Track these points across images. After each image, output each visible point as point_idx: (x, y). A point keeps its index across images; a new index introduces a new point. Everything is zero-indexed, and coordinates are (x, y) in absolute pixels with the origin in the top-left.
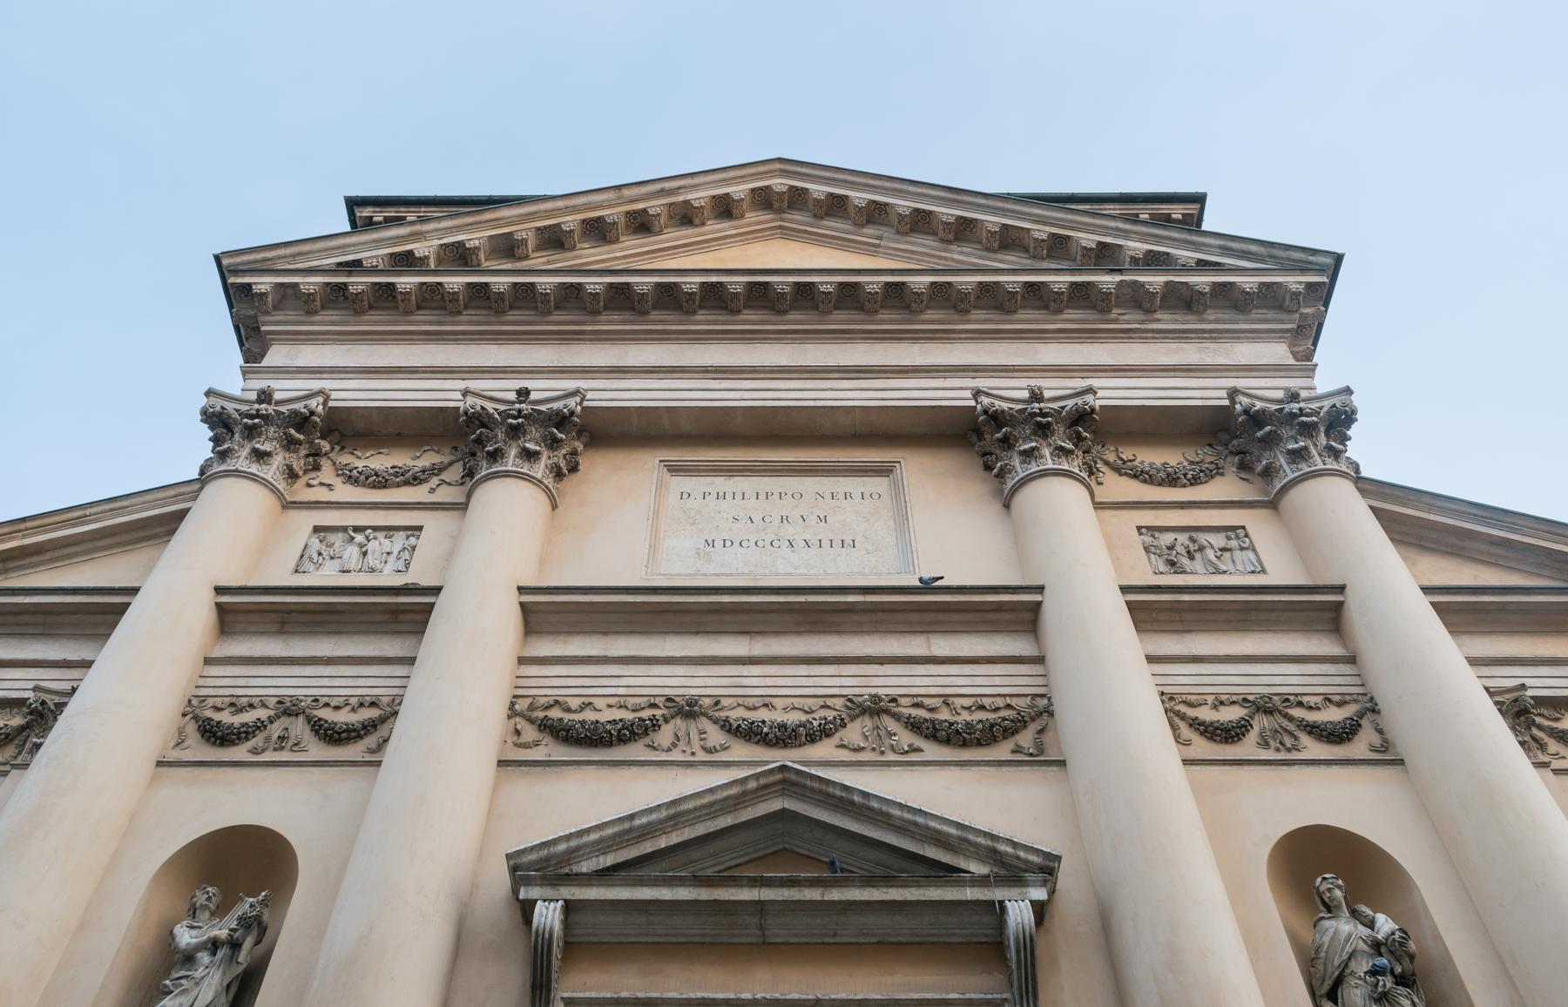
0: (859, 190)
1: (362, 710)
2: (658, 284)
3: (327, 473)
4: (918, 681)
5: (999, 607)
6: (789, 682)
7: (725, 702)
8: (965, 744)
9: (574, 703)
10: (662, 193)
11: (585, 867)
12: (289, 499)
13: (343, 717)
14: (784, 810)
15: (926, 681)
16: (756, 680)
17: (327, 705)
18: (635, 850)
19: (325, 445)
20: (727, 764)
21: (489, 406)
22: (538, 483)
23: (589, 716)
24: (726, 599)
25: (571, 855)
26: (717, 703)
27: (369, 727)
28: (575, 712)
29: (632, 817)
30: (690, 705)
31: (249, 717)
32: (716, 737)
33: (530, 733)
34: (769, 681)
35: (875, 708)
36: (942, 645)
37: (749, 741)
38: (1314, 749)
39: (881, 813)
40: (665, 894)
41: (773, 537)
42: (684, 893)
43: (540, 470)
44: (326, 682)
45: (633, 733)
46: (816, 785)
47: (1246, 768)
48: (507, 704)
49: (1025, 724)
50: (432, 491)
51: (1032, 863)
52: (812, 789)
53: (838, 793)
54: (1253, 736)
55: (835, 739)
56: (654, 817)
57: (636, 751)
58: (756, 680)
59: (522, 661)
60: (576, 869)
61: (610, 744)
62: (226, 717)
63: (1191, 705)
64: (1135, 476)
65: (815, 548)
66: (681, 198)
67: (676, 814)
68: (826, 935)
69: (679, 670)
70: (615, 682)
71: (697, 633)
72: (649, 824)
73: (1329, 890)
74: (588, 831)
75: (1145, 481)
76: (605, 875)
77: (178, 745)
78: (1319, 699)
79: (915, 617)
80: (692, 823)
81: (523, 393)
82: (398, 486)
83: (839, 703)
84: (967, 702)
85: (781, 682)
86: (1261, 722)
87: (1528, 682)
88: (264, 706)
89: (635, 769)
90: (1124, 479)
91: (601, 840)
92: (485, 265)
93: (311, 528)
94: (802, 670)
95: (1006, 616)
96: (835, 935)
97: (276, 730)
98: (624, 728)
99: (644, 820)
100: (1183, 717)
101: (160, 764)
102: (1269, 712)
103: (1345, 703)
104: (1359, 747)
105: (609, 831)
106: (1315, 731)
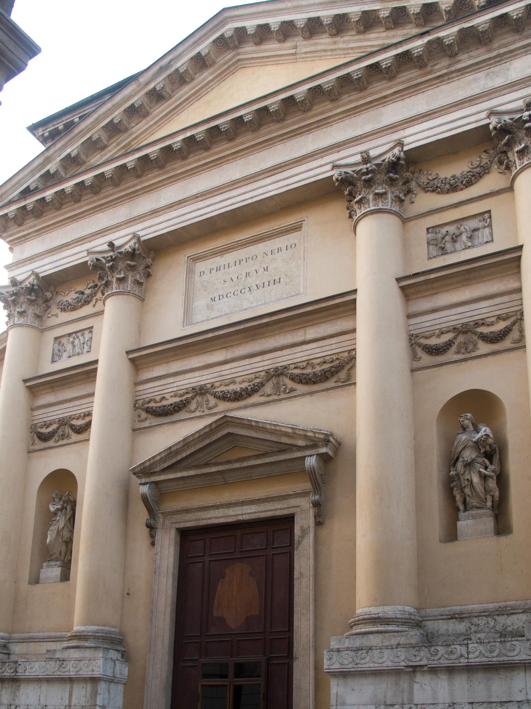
0: (274, 16)
2: (162, 149)
3: (54, 310)
4: (298, 355)
5: (337, 306)
6: (241, 369)
7: (216, 384)
8: (314, 383)
9: (158, 398)
10: (162, 70)
11: (158, 469)
13: (433, 341)
14: (229, 433)
15: (301, 354)
16: (227, 371)
17: (74, 419)
18: (176, 459)
19: (48, 295)
20: (215, 414)
21: (349, 170)
23: (165, 403)
24: (210, 335)
25: (152, 466)
26: (212, 386)
28: (158, 402)
29: (170, 448)
30: (200, 390)
31: (50, 429)
32: (213, 401)
33: (144, 415)
34: (233, 371)
35: (278, 373)
36: (312, 333)
37: (225, 401)
38: (484, 348)
39: (263, 428)
40: (185, 474)
41: (242, 287)
42: (192, 473)
43: (129, 285)
44: (71, 409)
45: (179, 407)
46: (238, 421)
48: (132, 405)
49: (343, 367)
50: (94, 306)
51: (321, 438)
52: (237, 423)
53: (246, 423)
55: (260, 393)
56: (178, 446)
57: (182, 415)
58: (227, 371)
60: (155, 470)
61: (172, 414)
62: (44, 430)
63: (426, 338)
64: (433, 191)
65: (261, 288)
66: (173, 69)
67: (186, 442)
68: (248, 477)
69: (197, 374)
70: (171, 386)
71: (204, 353)
72: (177, 449)
74: (156, 456)
75: (439, 193)
76: (164, 470)
77: (32, 444)
78: (494, 319)
79: (298, 320)
80: (195, 445)
81: (111, 245)
82: (81, 307)
83: (263, 374)
84: (318, 361)
85: (237, 370)
86: (461, 339)
87: (224, 373)
88: (55, 423)
89: (181, 423)
91: (161, 459)
92: (108, 144)
93: (53, 339)
94: (247, 361)
95: (341, 309)
96: (251, 477)
97: (60, 432)
98: (175, 406)
99: (175, 448)
101: (29, 452)
105: (163, 455)
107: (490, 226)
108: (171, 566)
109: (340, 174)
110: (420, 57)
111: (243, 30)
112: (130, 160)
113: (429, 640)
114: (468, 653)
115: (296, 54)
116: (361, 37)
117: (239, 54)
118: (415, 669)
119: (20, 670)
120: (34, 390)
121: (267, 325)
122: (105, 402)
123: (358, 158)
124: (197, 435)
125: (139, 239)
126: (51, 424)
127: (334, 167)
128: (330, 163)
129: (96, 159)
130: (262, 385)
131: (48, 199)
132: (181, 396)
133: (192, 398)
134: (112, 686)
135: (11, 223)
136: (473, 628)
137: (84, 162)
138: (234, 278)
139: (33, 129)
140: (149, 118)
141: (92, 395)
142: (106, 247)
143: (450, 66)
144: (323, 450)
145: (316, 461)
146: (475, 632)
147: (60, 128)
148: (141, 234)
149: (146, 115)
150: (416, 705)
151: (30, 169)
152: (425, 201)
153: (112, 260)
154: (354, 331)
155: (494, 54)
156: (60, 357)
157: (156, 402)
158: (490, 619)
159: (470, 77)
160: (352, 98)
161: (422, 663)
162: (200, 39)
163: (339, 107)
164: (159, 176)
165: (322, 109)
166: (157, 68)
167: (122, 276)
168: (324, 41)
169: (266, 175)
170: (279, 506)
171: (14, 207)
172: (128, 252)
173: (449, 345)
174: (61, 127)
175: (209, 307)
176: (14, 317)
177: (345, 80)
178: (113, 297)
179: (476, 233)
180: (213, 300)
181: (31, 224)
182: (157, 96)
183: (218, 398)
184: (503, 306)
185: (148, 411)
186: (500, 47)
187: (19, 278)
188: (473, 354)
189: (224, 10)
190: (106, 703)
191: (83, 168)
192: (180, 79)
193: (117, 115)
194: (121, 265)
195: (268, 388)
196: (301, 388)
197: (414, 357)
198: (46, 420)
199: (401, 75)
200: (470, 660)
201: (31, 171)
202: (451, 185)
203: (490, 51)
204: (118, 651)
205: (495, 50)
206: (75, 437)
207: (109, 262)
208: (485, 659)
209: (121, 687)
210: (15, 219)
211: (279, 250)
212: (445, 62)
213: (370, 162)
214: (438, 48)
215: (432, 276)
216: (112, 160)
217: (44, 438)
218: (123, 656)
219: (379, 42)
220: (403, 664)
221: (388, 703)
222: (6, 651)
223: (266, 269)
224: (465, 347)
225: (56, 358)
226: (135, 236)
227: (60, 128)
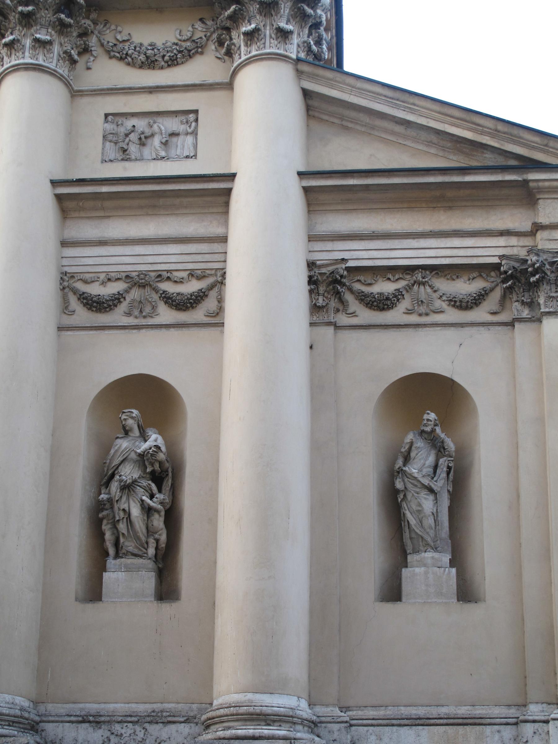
1: (110, 284)
12: (75, 88)
13: (95, 290)
17: (168, 278)
22: (52, 73)
27: (197, 299)
38: (166, 315)
47: (107, 332)
54: (123, 307)
59: (64, 244)
63: (86, 282)
64: (121, 59)
73: (125, 419)
75: (128, 64)
78: (184, 274)
86: (135, 294)
90: (114, 62)
100: (75, 291)
102: (143, 286)
103: (204, 277)
104: (198, 315)
106: (171, 301)
107: (195, 133)
152: (106, 72)
184: (199, 258)
197: (66, 309)
202: (148, 58)
215: (105, 189)
224: (139, 308)
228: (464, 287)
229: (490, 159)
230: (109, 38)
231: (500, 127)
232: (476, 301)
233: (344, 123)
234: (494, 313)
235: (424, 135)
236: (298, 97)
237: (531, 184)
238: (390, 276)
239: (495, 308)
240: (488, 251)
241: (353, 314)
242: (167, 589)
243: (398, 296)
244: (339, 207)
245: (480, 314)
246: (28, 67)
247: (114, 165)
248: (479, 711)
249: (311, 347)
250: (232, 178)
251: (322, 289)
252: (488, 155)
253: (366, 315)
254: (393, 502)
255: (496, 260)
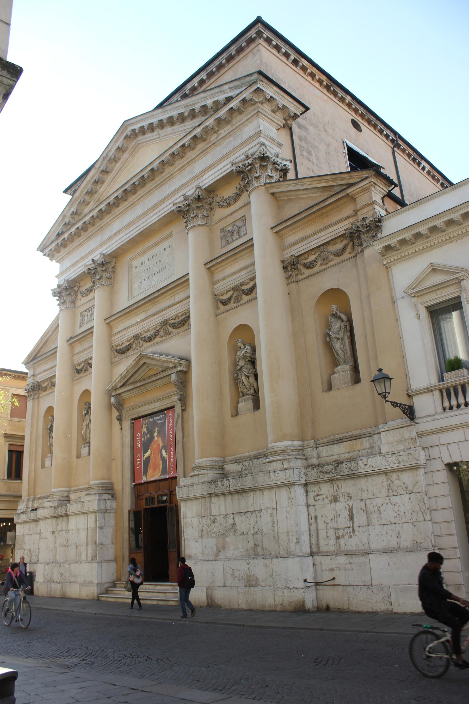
1: (228, 293)
3: (79, 296)
7: (142, 333)
9: (121, 344)
10: (104, 159)
13: (225, 297)
29: (121, 375)
35: (165, 323)
43: (104, 281)
54: (233, 301)
78: (248, 281)
81: (93, 260)
83: (159, 324)
87: (145, 326)
90: (220, 208)
94: (153, 318)
107: (245, 225)
108: (129, 441)
109: (176, 208)
110: (201, 137)
111: (134, 130)
112: (103, 206)
113: (224, 475)
114: (229, 484)
115: (159, 137)
116: (182, 125)
117: (138, 141)
118: (211, 495)
119: (68, 510)
120: (73, 345)
121: (158, 297)
122: (97, 351)
123: (182, 199)
124: (131, 366)
125: (200, 188)
126: (81, 364)
127: (174, 205)
128: (172, 202)
129: (86, 210)
130: (159, 331)
131: (155, 169)
132: (129, 341)
133: (133, 342)
134: (106, 514)
135: (97, 220)
136: (244, 468)
137: (81, 213)
138: (148, 269)
139: (66, 191)
140: (105, 184)
141: (188, 297)
142: (91, 262)
143: (217, 137)
144: (179, 369)
145: (175, 377)
146: (245, 470)
147: (195, 85)
148: (201, 185)
149: (103, 182)
150: (213, 516)
151: (58, 223)
152: (220, 213)
153: (188, 205)
154: (253, 264)
155: (234, 127)
156: (83, 323)
157: (120, 346)
158: (250, 462)
159: (227, 141)
160: (125, 204)
161: (212, 492)
162: (118, 139)
163: (176, 168)
164: (110, 217)
165: (168, 170)
166: (102, 158)
167: (258, 174)
168: (168, 129)
169: (151, 211)
170: (168, 402)
171: (54, 245)
172: (195, 199)
173: (230, 298)
174: (224, 61)
175: (140, 287)
176: (252, 182)
177: (173, 154)
178: (254, 191)
179: (241, 229)
180: (141, 282)
181: (64, 251)
182: (105, 172)
183: (145, 341)
185: (117, 351)
186: (236, 123)
187: (189, 194)
188: (241, 303)
189: (125, 122)
190: (103, 525)
191: (82, 216)
192: (114, 160)
193: (89, 187)
194: (99, 269)
195: (162, 333)
196: (175, 331)
197: (218, 308)
198: (79, 361)
199: (197, 146)
200: (231, 489)
201: (59, 224)
202: (228, 203)
203: (232, 125)
204: (109, 494)
205: (235, 125)
206: (245, 298)
207: (186, 207)
208: (236, 488)
209: (113, 514)
210: (55, 250)
211: (165, 249)
212: (215, 136)
213: (188, 200)
214: (207, 131)
216: (94, 209)
217: (79, 372)
218: (112, 496)
219: (190, 126)
220: (206, 493)
221: (202, 516)
222: (68, 499)
223: (160, 262)
224: (238, 300)
225: (82, 325)
226: (198, 187)
227: (195, 85)
228: (339, 246)
229: (337, 189)
230: (218, 199)
231: (333, 177)
232: (344, 250)
233: (289, 198)
234: (350, 253)
235: (313, 190)
236: (269, 197)
237: (350, 194)
238: (313, 253)
239: (350, 251)
240: (341, 228)
241: (303, 273)
242: (257, 406)
243: (316, 260)
244: (291, 233)
245: (346, 255)
246: (194, 227)
247: (226, 247)
248: (364, 431)
249: (289, 294)
250: (91, 335)
251: (289, 268)
252: (336, 188)
253: (307, 272)
254: (329, 346)
255: (344, 232)
